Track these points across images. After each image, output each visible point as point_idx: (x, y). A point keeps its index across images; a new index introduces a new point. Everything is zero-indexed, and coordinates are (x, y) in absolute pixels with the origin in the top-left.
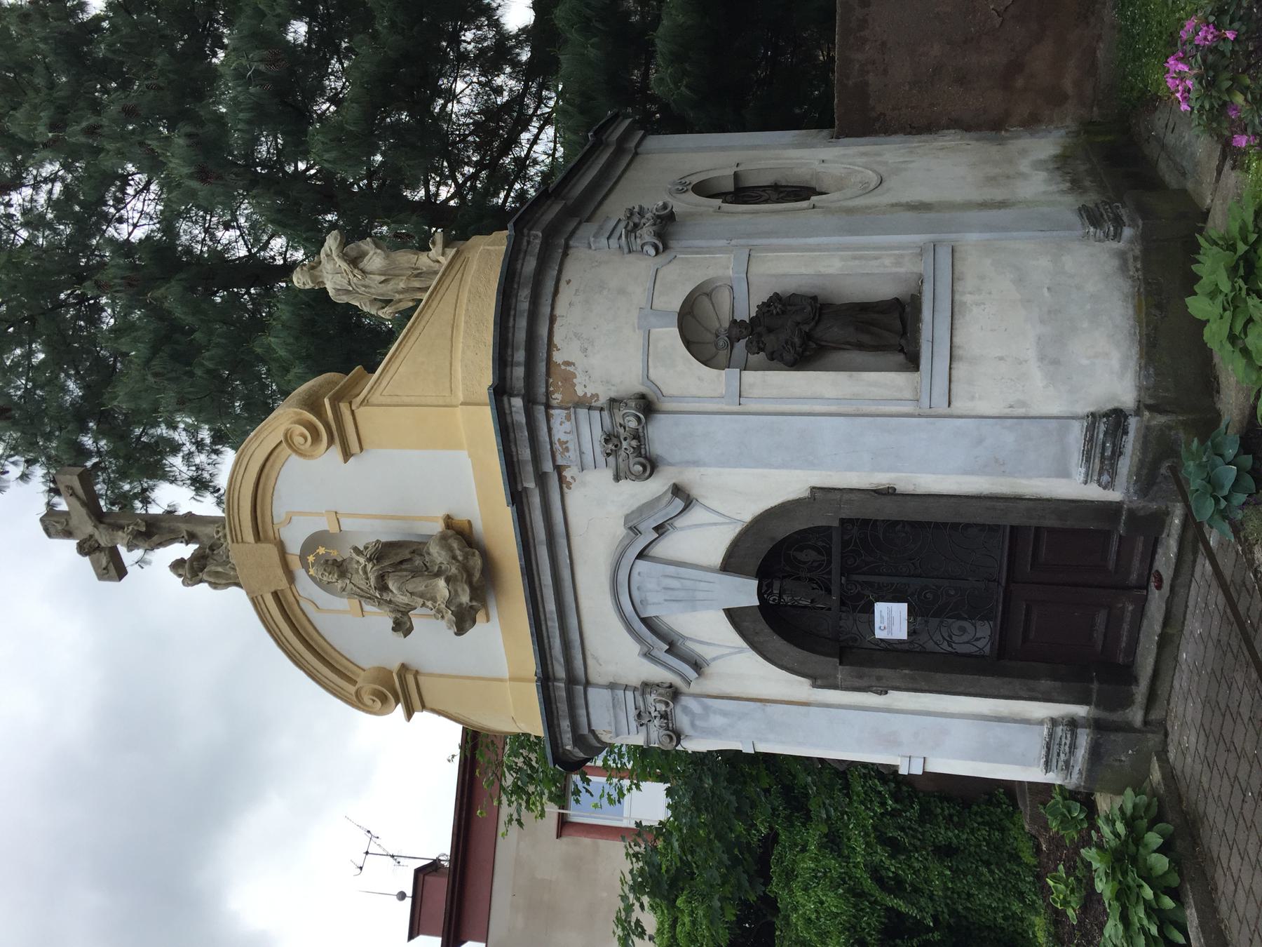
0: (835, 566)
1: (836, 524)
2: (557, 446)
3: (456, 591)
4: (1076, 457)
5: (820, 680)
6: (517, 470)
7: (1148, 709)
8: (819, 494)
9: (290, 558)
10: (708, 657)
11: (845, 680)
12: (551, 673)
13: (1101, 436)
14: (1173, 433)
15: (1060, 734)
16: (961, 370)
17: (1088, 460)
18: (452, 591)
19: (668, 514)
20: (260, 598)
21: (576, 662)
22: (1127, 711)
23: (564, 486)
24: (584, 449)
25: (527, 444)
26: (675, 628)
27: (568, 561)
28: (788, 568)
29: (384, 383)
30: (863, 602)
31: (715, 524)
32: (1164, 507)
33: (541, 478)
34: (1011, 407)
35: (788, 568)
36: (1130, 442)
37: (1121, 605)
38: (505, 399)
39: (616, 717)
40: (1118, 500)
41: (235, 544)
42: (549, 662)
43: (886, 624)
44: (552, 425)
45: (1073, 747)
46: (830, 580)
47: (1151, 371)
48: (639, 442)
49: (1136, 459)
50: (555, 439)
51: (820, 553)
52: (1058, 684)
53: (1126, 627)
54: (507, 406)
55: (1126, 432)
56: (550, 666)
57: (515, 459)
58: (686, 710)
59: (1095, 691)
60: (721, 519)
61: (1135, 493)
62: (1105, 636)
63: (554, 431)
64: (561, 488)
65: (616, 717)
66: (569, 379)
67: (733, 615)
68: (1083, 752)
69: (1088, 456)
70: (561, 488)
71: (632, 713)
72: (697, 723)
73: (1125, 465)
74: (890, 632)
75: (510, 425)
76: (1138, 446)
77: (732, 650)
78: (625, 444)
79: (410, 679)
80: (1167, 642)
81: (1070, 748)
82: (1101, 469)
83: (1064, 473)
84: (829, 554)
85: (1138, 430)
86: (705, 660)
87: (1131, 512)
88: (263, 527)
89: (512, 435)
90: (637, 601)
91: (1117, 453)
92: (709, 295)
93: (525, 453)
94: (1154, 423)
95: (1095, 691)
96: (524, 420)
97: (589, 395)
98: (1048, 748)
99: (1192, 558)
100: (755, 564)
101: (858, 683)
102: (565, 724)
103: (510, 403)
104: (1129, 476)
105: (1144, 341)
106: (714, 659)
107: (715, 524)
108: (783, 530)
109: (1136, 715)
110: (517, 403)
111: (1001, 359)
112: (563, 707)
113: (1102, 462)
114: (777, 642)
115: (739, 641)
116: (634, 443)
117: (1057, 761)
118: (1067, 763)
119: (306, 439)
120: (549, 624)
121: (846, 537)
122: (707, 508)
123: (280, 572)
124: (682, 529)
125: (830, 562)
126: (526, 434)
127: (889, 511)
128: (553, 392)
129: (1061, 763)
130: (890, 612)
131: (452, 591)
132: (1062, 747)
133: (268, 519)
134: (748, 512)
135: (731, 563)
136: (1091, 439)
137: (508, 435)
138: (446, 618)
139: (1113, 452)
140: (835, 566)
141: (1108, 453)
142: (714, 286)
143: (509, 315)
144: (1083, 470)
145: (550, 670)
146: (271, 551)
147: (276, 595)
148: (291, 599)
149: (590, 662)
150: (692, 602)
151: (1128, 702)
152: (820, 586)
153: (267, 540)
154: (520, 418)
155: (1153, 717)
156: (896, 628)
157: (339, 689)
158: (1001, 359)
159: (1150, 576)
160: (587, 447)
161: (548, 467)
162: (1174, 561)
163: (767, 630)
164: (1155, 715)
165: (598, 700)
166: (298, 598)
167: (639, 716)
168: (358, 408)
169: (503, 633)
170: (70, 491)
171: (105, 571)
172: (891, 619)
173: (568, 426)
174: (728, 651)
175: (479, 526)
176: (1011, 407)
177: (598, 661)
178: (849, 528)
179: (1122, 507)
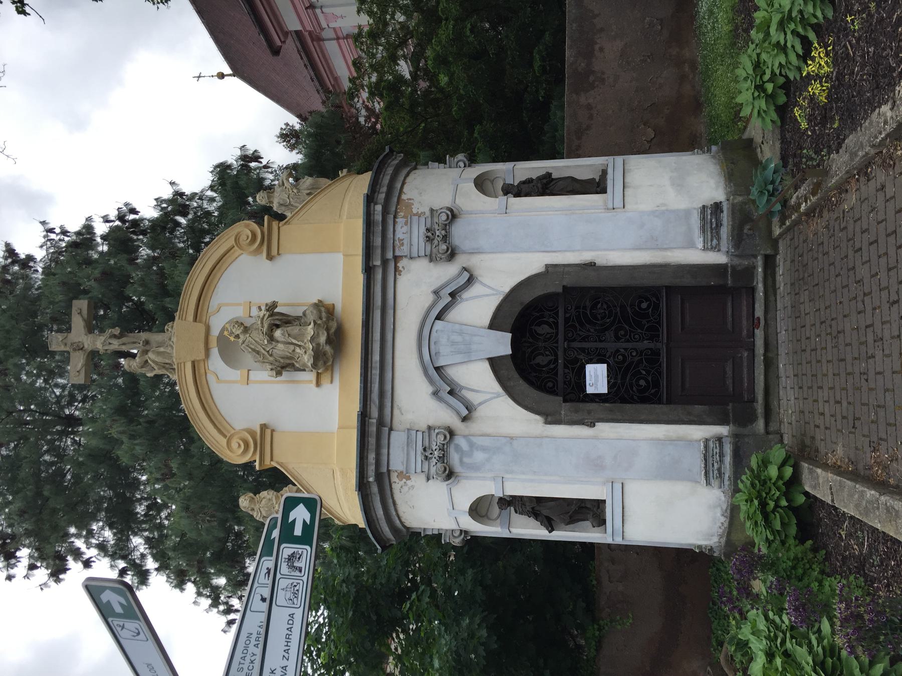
0: (561, 337)
1: (560, 290)
2: (397, 242)
3: (318, 333)
4: (697, 231)
5: (551, 418)
6: (371, 252)
7: (767, 424)
8: (551, 269)
9: (210, 338)
10: (476, 403)
11: (567, 416)
12: (368, 413)
13: (709, 217)
14: (747, 206)
15: (712, 446)
16: (628, 192)
17: (704, 232)
18: (316, 332)
19: (458, 283)
20: (182, 365)
21: (385, 409)
22: (754, 425)
23: (397, 273)
24: (413, 243)
25: (380, 235)
26: (456, 379)
27: (392, 326)
28: (531, 340)
29: (301, 214)
30: (579, 364)
31: (487, 295)
32: (751, 263)
33: (385, 262)
34: (658, 206)
35: (531, 340)
36: (725, 217)
37: (740, 355)
38: (372, 204)
39: (408, 454)
40: (725, 263)
41: (180, 320)
42: (368, 403)
43: (593, 381)
44: (396, 229)
45: (722, 455)
46: (557, 347)
47: (732, 184)
48: (446, 232)
49: (730, 227)
50: (397, 239)
51: (551, 328)
52: (706, 408)
53: (745, 370)
54: (372, 209)
55: (722, 212)
56: (368, 407)
57: (371, 244)
58: (458, 448)
59: (730, 411)
60: (489, 291)
61: (732, 247)
62: (733, 382)
63: (397, 232)
64: (395, 275)
65: (408, 454)
66: (409, 206)
67: (495, 363)
68: (729, 458)
69: (703, 229)
70: (395, 275)
71: (420, 448)
72: (466, 460)
73: (725, 231)
74: (596, 388)
75: (372, 222)
76: (730, 219)
77: (493, 395)
78: (438, 233)
79: (268, 432)
80: (770, 364)
81: (720, 456)
82: (712, 236)
83: (691, 245)
84: (557, 328)
85: (728, 209)
86: (473, 405)
87: (733, 267)
88: (201, 312)
89: (372, 228)
90: (433, 353)
91: (719, 225)
92: (492, 182)
93: (378, 241)
94: (735, 201)
95: (730, 411)
96: (381, 219)
97: (420, 213)
98: (706, 460)
99: (774, 298)
100: (511, 321)
101: (576, 417)
102: (372, 457)
103: (374, 208)
104: (728, 239)
105: (727, 176)
106: (480, 404)
107: (487, 295)
108: (528, 297)
109: (760, 424)
110: (379, 208)
111: (651, 186)
112: (372, 441)
113: (711, 233)
114: (522, 385)
115: (496, 387)
116: (443, 232)
117: (713, 471)
118: (719, 470)
119: (248, 238)
120: (374, 372)
121: (568, 315)
122: (485, 285)
123: (202, 346)
124: (467, 300)
125: (557, 334)
126: (381, 228)
127: (590, 280)
128: (399, 212)
129: (716, 472)
130: (596, 370)
131: (316, 332)
132: (715, 457)
133: (206, 307)
134: (507, 285)
135: (494, 325)
136: (704, 218)
137: (370, 228)
138: (308, 354)
139: (717, 225)
140: (561, 337)
141: (714, 226)
142: (498, 176)
143: (381, 172)
144: (702, 239)
145: (368, 410)
146: (201, 327)
147: (193, 363)
148: (202, 371)
149: (396, 412)
150: (468, 358)
151: (752, 419)
152: (551, 354)
153: (200, 322)
154: (378, 217)
155: (772, 429)
156: (600, 383)
157: (215, 442)
158: (651, 186)
159: (754, 323)
160: (415, 240)
161: (390, 255)
162: (763, 297)
163: (516, 375)
164: (773, 427)
165: (398, 439)
166: (207, 371)
167: (425, 450)
168: (283, 225)
169: (340, 389)
170: (79, 311)
171: (77, 374)
172: (596, 376)
173: (405, 229)
174: (488, 396)
175: (339, 308)
176: (658, 206)
177: (401, 411)
178: (569, 308)
179: (728, 265)
